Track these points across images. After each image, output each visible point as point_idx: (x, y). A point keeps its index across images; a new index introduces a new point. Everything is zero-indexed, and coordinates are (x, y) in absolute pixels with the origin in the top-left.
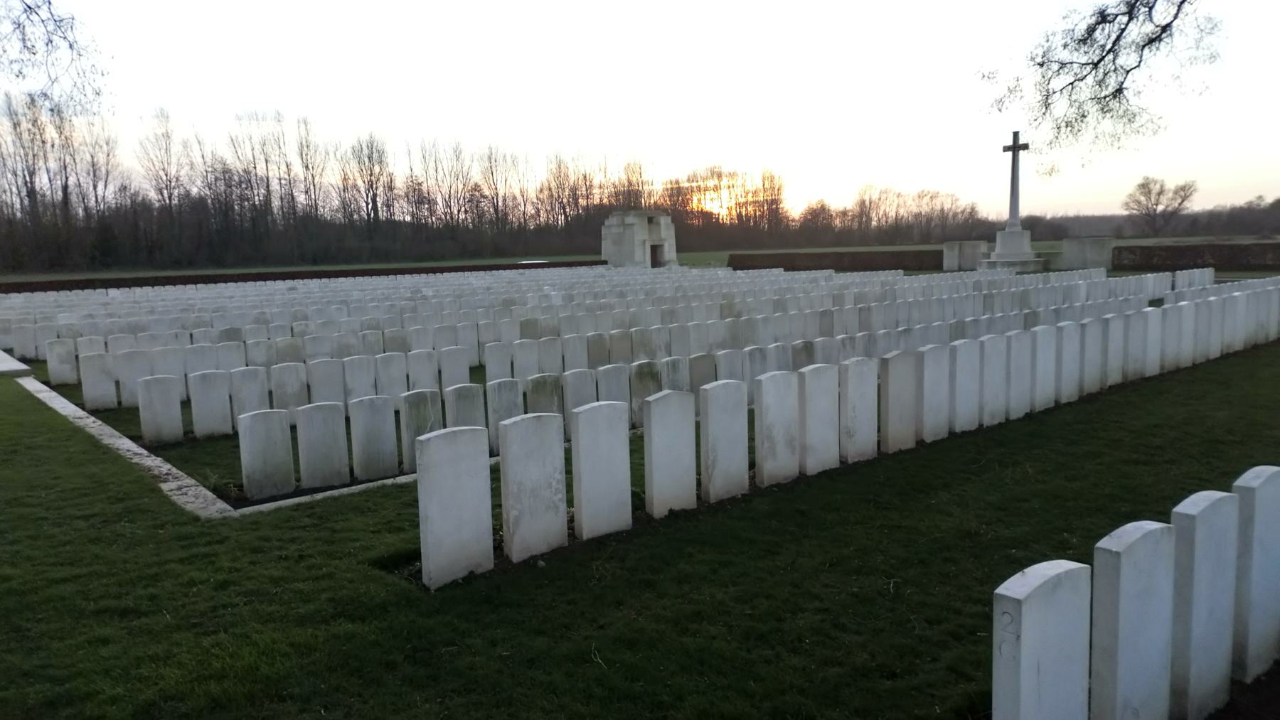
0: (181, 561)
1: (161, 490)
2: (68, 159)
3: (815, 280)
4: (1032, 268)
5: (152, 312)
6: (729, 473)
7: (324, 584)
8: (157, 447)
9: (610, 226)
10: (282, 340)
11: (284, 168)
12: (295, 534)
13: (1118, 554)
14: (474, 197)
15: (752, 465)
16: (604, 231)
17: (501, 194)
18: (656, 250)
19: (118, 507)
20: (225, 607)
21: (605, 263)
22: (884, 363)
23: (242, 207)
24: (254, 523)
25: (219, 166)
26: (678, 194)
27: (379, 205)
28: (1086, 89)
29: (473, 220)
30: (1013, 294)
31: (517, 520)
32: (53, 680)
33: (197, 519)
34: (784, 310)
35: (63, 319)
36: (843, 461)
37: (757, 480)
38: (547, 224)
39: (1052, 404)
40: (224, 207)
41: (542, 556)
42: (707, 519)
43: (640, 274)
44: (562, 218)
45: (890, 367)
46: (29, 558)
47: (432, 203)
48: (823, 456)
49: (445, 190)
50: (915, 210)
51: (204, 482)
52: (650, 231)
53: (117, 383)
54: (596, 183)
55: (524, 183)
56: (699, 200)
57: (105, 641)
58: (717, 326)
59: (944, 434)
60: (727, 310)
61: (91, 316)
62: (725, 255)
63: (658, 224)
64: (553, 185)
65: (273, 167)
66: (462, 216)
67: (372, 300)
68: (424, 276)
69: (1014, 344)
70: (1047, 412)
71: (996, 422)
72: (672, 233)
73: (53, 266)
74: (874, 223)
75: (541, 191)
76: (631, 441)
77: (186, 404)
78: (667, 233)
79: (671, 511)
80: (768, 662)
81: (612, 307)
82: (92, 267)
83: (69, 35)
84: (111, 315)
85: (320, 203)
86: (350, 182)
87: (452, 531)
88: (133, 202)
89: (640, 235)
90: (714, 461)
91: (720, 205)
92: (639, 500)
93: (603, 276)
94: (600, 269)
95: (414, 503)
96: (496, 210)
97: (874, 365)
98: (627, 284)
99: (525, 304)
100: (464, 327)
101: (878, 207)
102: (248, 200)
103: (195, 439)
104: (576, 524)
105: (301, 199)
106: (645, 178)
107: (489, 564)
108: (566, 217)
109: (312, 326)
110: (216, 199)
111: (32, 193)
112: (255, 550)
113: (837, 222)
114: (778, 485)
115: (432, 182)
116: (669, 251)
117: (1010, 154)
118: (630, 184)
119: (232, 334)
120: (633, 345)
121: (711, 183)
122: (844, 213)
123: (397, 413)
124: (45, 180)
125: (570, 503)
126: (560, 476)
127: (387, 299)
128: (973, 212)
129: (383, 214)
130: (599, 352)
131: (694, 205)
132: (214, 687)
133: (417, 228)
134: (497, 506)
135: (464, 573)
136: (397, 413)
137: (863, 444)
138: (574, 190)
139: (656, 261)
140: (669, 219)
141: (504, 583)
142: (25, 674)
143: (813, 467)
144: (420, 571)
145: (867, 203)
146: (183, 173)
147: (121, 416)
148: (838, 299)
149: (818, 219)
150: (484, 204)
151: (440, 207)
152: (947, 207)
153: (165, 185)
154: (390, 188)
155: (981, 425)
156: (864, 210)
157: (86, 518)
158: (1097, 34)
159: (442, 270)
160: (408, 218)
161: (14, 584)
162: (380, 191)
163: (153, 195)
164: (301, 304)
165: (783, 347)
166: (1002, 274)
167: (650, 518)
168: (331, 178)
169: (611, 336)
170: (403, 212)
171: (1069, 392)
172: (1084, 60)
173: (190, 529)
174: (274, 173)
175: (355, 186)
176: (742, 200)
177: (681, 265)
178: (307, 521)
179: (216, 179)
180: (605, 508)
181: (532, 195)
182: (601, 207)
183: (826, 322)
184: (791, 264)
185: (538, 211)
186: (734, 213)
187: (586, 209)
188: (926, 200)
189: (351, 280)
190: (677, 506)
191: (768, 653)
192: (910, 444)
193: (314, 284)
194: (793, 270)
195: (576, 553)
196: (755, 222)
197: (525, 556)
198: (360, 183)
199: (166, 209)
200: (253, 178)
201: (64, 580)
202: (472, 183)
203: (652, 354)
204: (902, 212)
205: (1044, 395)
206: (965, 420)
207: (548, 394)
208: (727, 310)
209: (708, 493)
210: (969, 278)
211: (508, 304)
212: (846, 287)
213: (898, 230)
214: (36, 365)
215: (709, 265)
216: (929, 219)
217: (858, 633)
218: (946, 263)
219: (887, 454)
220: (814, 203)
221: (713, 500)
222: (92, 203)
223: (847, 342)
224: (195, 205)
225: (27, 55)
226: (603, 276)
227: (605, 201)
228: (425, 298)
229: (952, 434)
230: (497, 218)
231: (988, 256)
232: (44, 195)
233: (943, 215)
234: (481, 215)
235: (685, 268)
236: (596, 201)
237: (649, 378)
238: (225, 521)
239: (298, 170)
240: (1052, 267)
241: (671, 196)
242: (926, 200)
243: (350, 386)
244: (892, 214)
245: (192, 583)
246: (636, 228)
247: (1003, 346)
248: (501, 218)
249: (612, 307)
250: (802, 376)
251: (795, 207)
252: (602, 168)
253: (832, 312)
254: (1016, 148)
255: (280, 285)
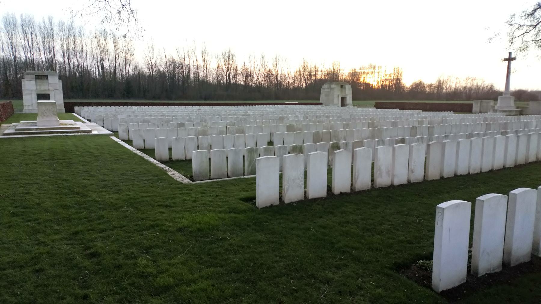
0: (180, 194)
1: (168, 175)
2: (117, 56)
3: (413, 114)
4: (514, 113)
5: (151, 116)
6: (363, 181)
7: (226, 203)
8: (162, 162)
9: (324, 89)
10: (200, 128)
11: (195, 61)
12: (214, 189)
13: (483, 201)
14: (269, 75)
15: (372, 181)
16: (322, 90)
17: (280, 74)
18: (343, 99)
19: (156, 178)
20: (196, 207)
21: (321, 104)
22: (429, 145)
23: (179, 77)
24: (200, 186)
25: (171, 60)
26: (355, 75)
27: (231, 77)
28: (530, 37)
29: (268, 84)
30: (500, 124)
31: (287, 190)
32: (152, 221)
33: (182, 183)
34: (396, 126)
35: (120, 117)
36: (409, 182)
37: (374, 185)
38: (298, 86)
39: (502, 168)
40: (172, 76)
41: (295, 202)
42: (353, 196)
43: (335, 109)
44: (304, 85)
45: (431, 147)
46: (133, 190)
47: (252, 77)
48: (401, 179)
49: (257, 72)
50: (464, 85)
51: (180, 173)
52: (341, 91)
53: (144, 140)
54: (319, 70)
55: (289, 68)
56: (364, 78)
57: (163, 213)
58: (366, 130)
59: (452, 175)
60: (371, 124)
61: (130, 116)
62: (373, 102)
63: (345, 88)
64: (301, 70)
65: (191, 61)
66: (263, 83)
67: (229, 115)
68: (248, 106)
69: (486, 141)
70: (499, 170)
71: (476, 172)
72: (351, 92)
73: (110, 96)
74: (444, 90)
75: (296, 72)
76: (328, 170)
77: (170, 149)
78: (348, 92)
79: (341, 193)
80: (369, 236)
81: (323, 122)
82: (123, 97)
83: (135, 15)
84: (136, 116)
85: (209, 76)
86: (220, 68)
87: (266, 192)
88: (139, 73)
89: (337, 93)
90: (358, 176)
91: (374, 80)
92: (329, 188)
93: (320, 109)
94: (319, 106)
95: (255, 180)
96: (277, 80)
97: (424, 146)
98: (330, 113)
99: (288, 119)
100: (265, 126)
101: (447, 83)
102: (181, 74)
103: (172, 161)
104: (307, 194)
105: (201, 74)
106: (340, 68)
107: (277, 202)
108: (306, 84)
109: (209, 124)
110: (169, 73)
111: (103, 68)
112: (202, 193)
113: (427, 89)
114: (382, 188)
115: (252, 68)
116: (349, 100)
117: (507, 62)
118: (334, 70)
119: (181, 125)
120: (331, 135)
121: (370, 70)
122: (431, 86)
123: (244, 156)
124: (108, 63)
125: (305, 187)
126: (302, 176)
127: (235, 115)
128: (492, 87)
129: (232, 81)
130: (317, 138)
131: (362, 80)
132: (198, 225)
133: (245, 87)
134: (281, 187)
135: (269, 205)
136: (244, 156)
137: (418, 175)
138: (310, 73)
139: (343, 104)
140: (350, 86)
141: (281, 209)
142: (143, 219)
143: (397, 182)
144: (255, 203)
145: (442, 81)
146: (158, 62)
147: (150, 152)
148: (421, 123)
149: (418, 89)
150: (273, 78)
151: (255, 79)
152: (479, 84)
153: (151, 66)
154: (236, 70)
155: (469, 173)
156: (440, 85)
157: (148, 180)
158: (536, 14)
159: (255, 104)
160: (242, 83)
161: (132, 196)
162: (232, 71)
163: (146, 71)
164: (203, 115)
165: (392, 140)
166: (499, 115)
167: (333, 194)
168: (212, 66)
169: (322, 133)
170: (240, 81)
171: (510, 163)
172: (529, 24)
173: (180, 186)
174: (191, 63)
175: (222, 69)
176: (384, 78)
177: (354, 106)
178: (217, 186)
179: (170, 65)
180: (317, 189)
181: (292, 74)
182: (321, 80)
183: (413, 131)
184: (402, 107)
185: (294, 81)
186: (380, 84)
187: (315, 81)
188: (470, 80)
189: (220, 107)
190: (343, 191)
191: (370, 234)
192: (438, 178)
193: (207, 108)
194: (403, 109)
195: (306, 204)
196: (389, 88)
197: (289, 202)
198: (224, 68)
199: (151, 77)
200: (184, 66)
201: (146, 197)
202: (268, 69)
203: (339, 140)
204: (458, 86)
205: (498, 164)
206: (462, 170)
207: (299, 149)
208: (371, 124)
209: (355, 187)
210: (483, 116)
211: (281, 119)
212: (426, 118)
213: (456, 94)
214: (116, 133)
215: (365, 106)
216: (471, 89)
217: (402, 232)
218: (474, 109)
219: (428, 181)
220: (417, 81)
221: (357, 190)
222: (124, 73)
223: (420, 139)
224: (162, 75)
225: (120, 22)
226: (320, 109)
227: (323, 77)
228: (249, 115)
229: (456, 175)
230: (278, 83)
231: (494, 107)
232: (107, 69)
233: (477, 88)
234: (271, 82)
235: (355, 107)
236: (319, 77)
237: (336, 147)
238: (186, 185)
239: (201, 63)
240: (524, 113)
241: (352, 76)
242: (470, 80)
243: (225, 145)
244: (453, 86)
245: (185, 200)
246: (335, 90)
247: (481, 142)
248: (279, 84)
249: (323, 122)
250: (394, 148)
251: (407, 83)
252: (323, 66)
253: (416, 127)
254: (510, 59)
255: (194, 108)
